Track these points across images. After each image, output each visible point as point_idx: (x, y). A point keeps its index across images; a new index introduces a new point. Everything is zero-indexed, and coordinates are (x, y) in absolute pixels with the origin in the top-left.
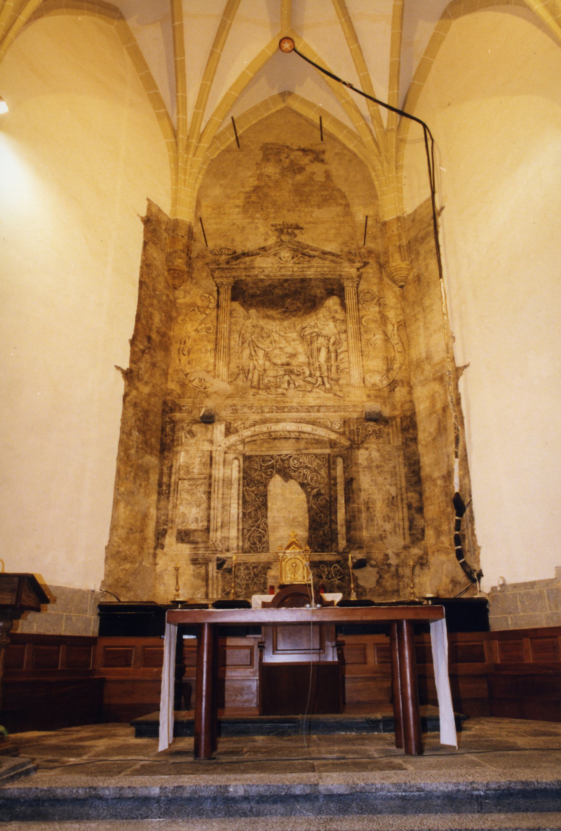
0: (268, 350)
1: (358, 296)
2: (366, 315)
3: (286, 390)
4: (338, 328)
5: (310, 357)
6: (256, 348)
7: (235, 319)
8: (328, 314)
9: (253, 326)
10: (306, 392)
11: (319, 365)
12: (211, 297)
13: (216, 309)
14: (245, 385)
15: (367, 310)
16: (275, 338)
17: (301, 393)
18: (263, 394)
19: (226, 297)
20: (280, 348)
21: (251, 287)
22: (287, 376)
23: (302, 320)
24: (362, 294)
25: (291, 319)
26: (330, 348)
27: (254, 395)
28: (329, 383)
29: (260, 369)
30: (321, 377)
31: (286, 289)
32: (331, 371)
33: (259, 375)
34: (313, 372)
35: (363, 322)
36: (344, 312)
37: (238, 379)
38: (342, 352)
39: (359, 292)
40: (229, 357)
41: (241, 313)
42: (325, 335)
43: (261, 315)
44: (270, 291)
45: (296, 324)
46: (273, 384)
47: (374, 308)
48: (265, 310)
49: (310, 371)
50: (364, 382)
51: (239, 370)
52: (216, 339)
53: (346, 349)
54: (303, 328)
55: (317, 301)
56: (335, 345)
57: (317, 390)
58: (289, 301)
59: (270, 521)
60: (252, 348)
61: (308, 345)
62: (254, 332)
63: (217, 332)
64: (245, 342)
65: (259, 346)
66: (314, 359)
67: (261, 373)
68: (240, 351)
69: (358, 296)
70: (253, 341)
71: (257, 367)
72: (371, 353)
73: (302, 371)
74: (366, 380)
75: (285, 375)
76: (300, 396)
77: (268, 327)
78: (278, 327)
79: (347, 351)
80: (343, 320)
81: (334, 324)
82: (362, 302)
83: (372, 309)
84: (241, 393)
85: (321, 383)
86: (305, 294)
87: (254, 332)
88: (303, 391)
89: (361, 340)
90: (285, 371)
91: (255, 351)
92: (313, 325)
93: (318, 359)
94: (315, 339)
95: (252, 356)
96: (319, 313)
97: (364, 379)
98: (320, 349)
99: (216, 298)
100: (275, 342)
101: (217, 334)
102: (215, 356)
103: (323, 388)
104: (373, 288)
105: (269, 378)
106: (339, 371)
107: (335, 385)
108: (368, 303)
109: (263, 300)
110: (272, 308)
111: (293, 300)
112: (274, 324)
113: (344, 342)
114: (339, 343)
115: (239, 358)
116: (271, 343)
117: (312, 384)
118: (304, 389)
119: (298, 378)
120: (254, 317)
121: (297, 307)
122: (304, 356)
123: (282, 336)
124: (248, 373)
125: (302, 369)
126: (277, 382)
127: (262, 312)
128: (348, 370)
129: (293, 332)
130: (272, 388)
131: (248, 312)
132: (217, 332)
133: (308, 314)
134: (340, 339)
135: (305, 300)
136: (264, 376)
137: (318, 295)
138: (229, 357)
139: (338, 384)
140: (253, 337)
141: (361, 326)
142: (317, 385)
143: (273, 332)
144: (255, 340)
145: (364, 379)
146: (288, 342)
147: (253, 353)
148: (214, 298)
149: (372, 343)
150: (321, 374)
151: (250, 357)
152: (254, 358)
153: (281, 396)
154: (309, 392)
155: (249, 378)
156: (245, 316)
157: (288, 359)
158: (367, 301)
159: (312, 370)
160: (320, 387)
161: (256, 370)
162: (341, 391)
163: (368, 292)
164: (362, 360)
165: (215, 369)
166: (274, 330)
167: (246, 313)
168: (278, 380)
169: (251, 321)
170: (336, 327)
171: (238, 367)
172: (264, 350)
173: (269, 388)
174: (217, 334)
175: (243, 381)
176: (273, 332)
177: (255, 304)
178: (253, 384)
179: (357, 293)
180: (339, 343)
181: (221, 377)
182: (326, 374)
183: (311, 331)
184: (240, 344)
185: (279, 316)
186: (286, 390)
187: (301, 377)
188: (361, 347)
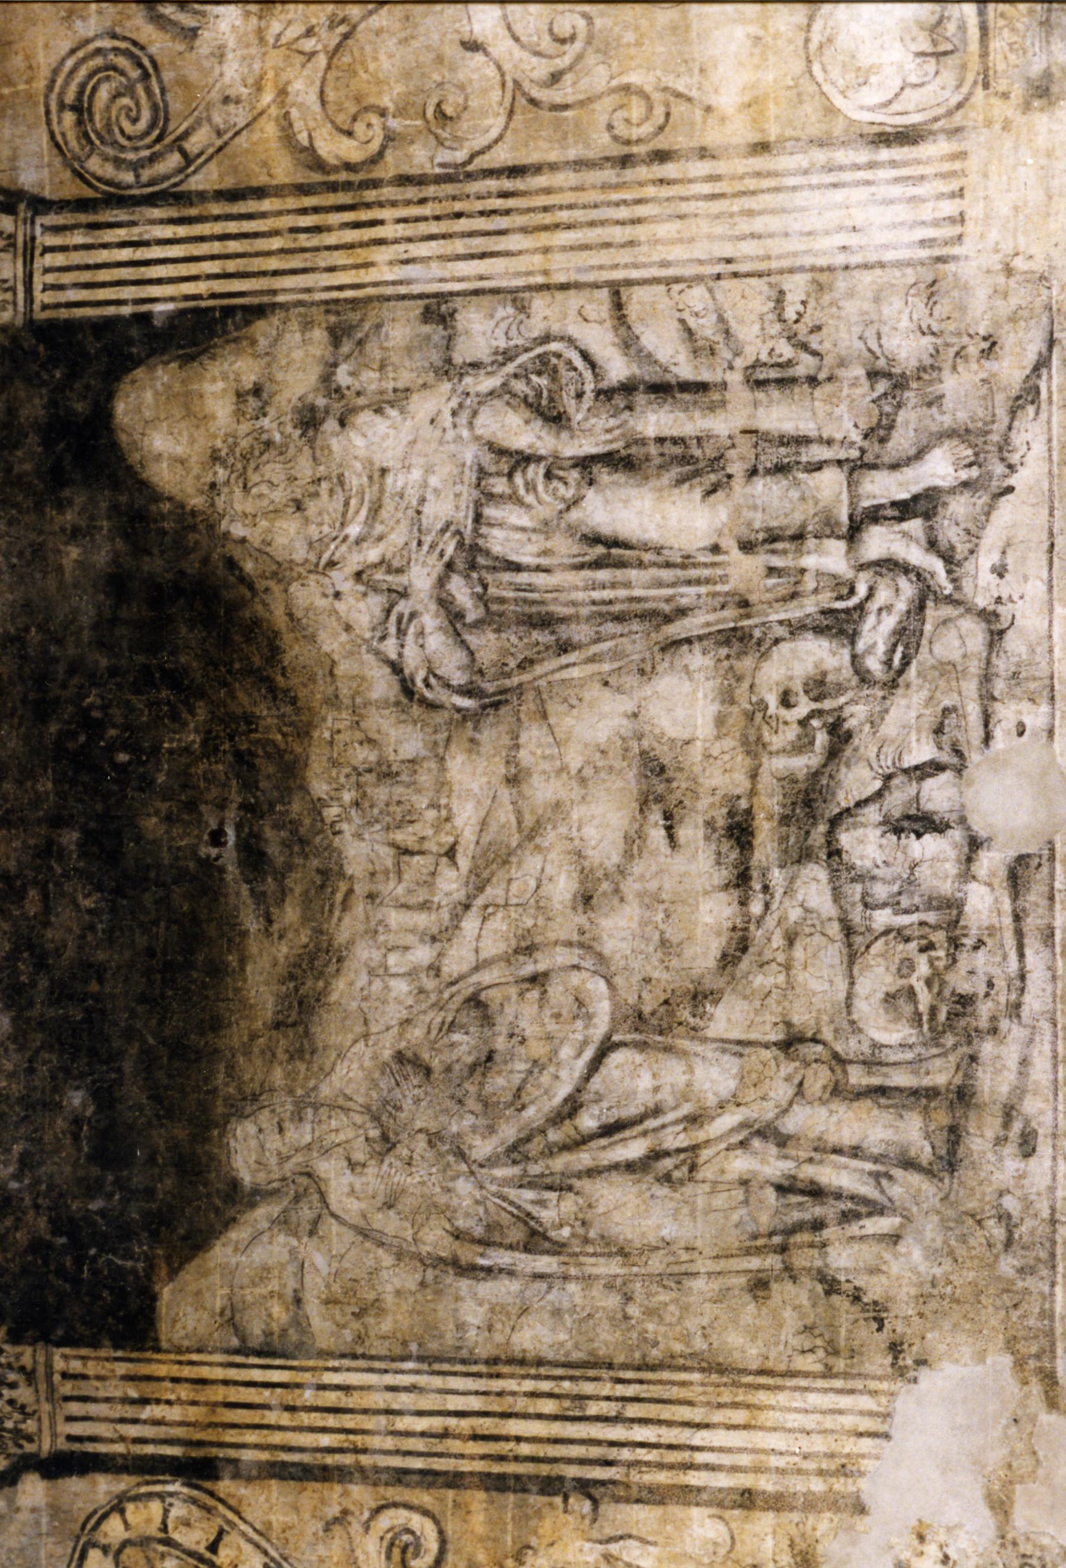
0: (603, 1010)
1: (118, 199)
2: (286, 124)
3: (974, 844)
4: (405, 378)
5: (676, 629)
6: (588, 1121)
7: (313, 1308)
8: (274, 470)
9: (387, 1144)
10: (1001, 665)
11: (747, 547)
12: (114, 1530)
13: (225, 1486)
14: (931, 1229)
15: (239, 116)
16: (491, 948)
17: (1006, 714)
18: (1011, 1054)
19: (115, 1389)
20: (586, 900)
21: (25, 1162)
22: (845, 839)
23: (333, 701)
24: (94, 164)
25: (317, 807)
26: (588, 447)
27: (1027, 1146)
28: (919, 455)
29: (782, 1092)
30: (853, 533)
31: (48, 850)
32: (803, 441)
33: (837, 1091)
34: (809, 607)
35: (350, 150)
36: (263, 329)
37: (875, 1289)
38: (629, 344)
39: (73, 190)
40: (668, 1363)
41: (259, 1255)
42: (468, 494)
43: (278, 1076)
44: (61, 994)
45: (363, 755)
46: (923, 969)
47: (220, 54)
48: (235, 1036)
49: (796, 629)
50: (907, 137)
51: (790, 1273)
52: (497, 1484)
53: (599, 305)
54: (408, 689)
55: (155, 565)
56: (569, 403)
57: (987, 559)
58: (151, 824)
59: (724, 941)
60: (584, 1158)
61: (564, 647)
62: (434, 1138)
63: (430, 1478)
64: (525, 1218)
65: (564, 1091)
66: (688, 595)
67: (819, 1079)
68: (613, 1267)
69: (118, 199)
70: (516, 1152)
71: (767, 1112)
72: (634, 78)
73: (804, 707)
74: (892, 121)
75: (834, 852)
76: (1036, 717)
77: (394, 1013)
78: (395, 918)
79: (617, 293)
80: (336, 335)
81: (364, 418)
82: (174, 160)
83: (232, 71)
84: (1007, 1265)
85: (915, 526)
86: (94, 679)
87: (434, 1138)
88: (987, 698)
89: (516, 171)
90: (805, 856)
91: (611, 1130)
92: (376, 603)
93: (687, 561)
94: (501, 586)
95: (657, 1155)
96: (262, 552)
97: (884, 139)
98: (595, 539)
99: (124, 1483)
100: (528, 949)
101: (455, 1480)
102: (655, 1496)
103: (959, 507)
104: (44, 62)
105: (867, 1008)
106: (806, 365)
107: (935, 402)
108: (176, 106)
109: (148, 1060)
110: (217, 971)
111: (147, 783)
112: (364, 953)
113: (536, 327)
114: (544, 365)
115: (680, 1278)
116: (537, 980)
117: (919, 607)
118: (971, 687)
119: (865, 743)
120: (302, 1134)
121: (210, 747)
122: (667, 683)
123: (479, 882)
124: (816, 1192)
125: (786, 700)
126: (902, 935)
127: (251, 1070)
128: (796, 287)
129: (443, 785)
130: (959, 982)
131: (256, 1196)
132: (430, 1478)
133: (274, 652)
134: (507, 356)
135: (145, 680)
136: (849, 1047)
137: (102, 558)
138: (668, 1363)
139: (930, 370)
140: (482, 1148)
141: (390, 167)
142: (938, 566)
143: (435, 970)
144: (509, 1132)
145: (884, 139)
146: (531, 834)
147: (634, 1149)
148: (118, 1507)
149: (541, 69)
150: (828, 528)
151: (667, 1178)
152: (675, 1139)
153: (1034, 896)
154: (996, 636)
155: (867, 1190)
156: (283, 1222)
157: (690, 832)
158: (160, 115)
159: (794, 612)
160: (950, 533)
161: (790, 1125)
162: (991, 347)
163: (81, 109)
164: (704, 153)
165: (778, 1503)
166: (423, 954)
167: (263, 1213)
168: (882, 918)
169: (329, 1168)
170: (400, 398)
171: (759, 1286)
172: (606, 1048)
173: (965, 1001)
174: (455, 1480)
175: (895, 1238)
176: (435, 970)
177: (181, 1132)
178: (925, 1152)
179: (82, 205)
180: (544, 365)
181: (851, 1446)
182: (831, 482)
183: (430, 620)
184: (545, 1263)
185: (291, 913)
186: (974, 844)
187: (857, 715)
188: (579, 164)
